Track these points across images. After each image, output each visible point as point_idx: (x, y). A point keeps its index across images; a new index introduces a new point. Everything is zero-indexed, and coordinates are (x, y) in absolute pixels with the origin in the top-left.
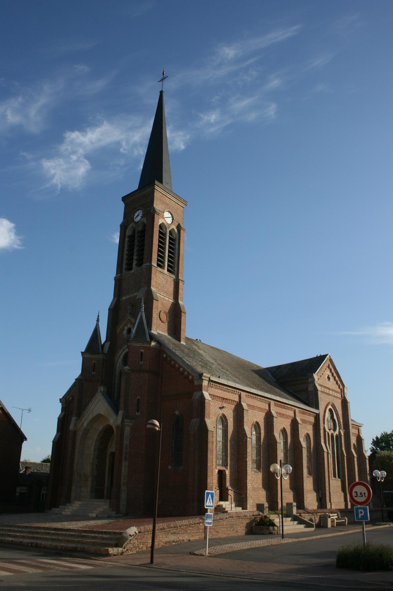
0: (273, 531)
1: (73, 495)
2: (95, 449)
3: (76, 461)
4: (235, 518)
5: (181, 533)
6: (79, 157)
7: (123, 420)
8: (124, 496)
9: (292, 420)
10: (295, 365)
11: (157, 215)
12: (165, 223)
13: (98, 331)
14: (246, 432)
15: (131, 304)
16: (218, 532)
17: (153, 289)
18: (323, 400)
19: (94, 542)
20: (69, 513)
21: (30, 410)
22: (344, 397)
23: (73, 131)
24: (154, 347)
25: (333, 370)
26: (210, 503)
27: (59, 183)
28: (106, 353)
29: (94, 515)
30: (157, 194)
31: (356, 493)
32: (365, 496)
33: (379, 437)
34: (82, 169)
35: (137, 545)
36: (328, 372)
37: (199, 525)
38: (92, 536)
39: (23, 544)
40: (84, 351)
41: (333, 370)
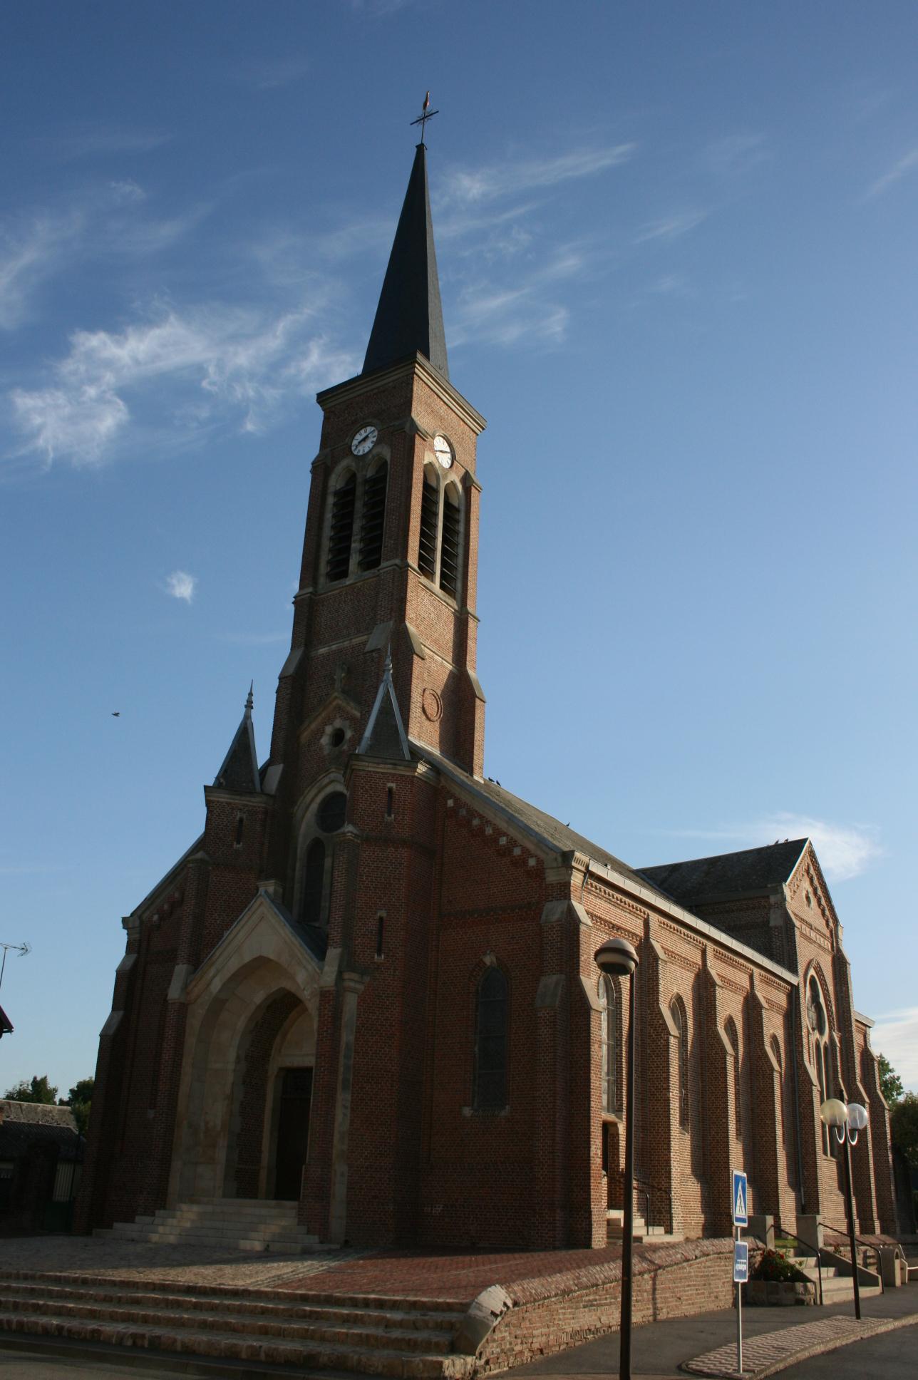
0: (805, 1294)
1: (175, 1185)
2: (238, 1057)
3: (184, 1089)
4: (711, 1257)
6: (104, 392)
7: (340, 973)
8: (339, 1190)
9: (745, 998)
10: (720, 863)
11: (420, 438)
13: (250, 730)
15: (344, 666)
16: (680, 1299)
17: (411, 628)
18: (805, 952)
19: (367, 1336)
20: (172, 1239)
21: (25, 950)
22: (839, 950)
23: (92, 328)
24: (423, 778)
25: (815, 878)
27: (50, 449)
28: (273, 792)
29: (258, 1246)
30: (419, 389)
34: (109, 420)
35: (508, 1346)
36: (806, 885)
37: (641, 1280)
38: (342, 1315)
39: (102, 1338)
40: (211, 785)
41: (815, 878)
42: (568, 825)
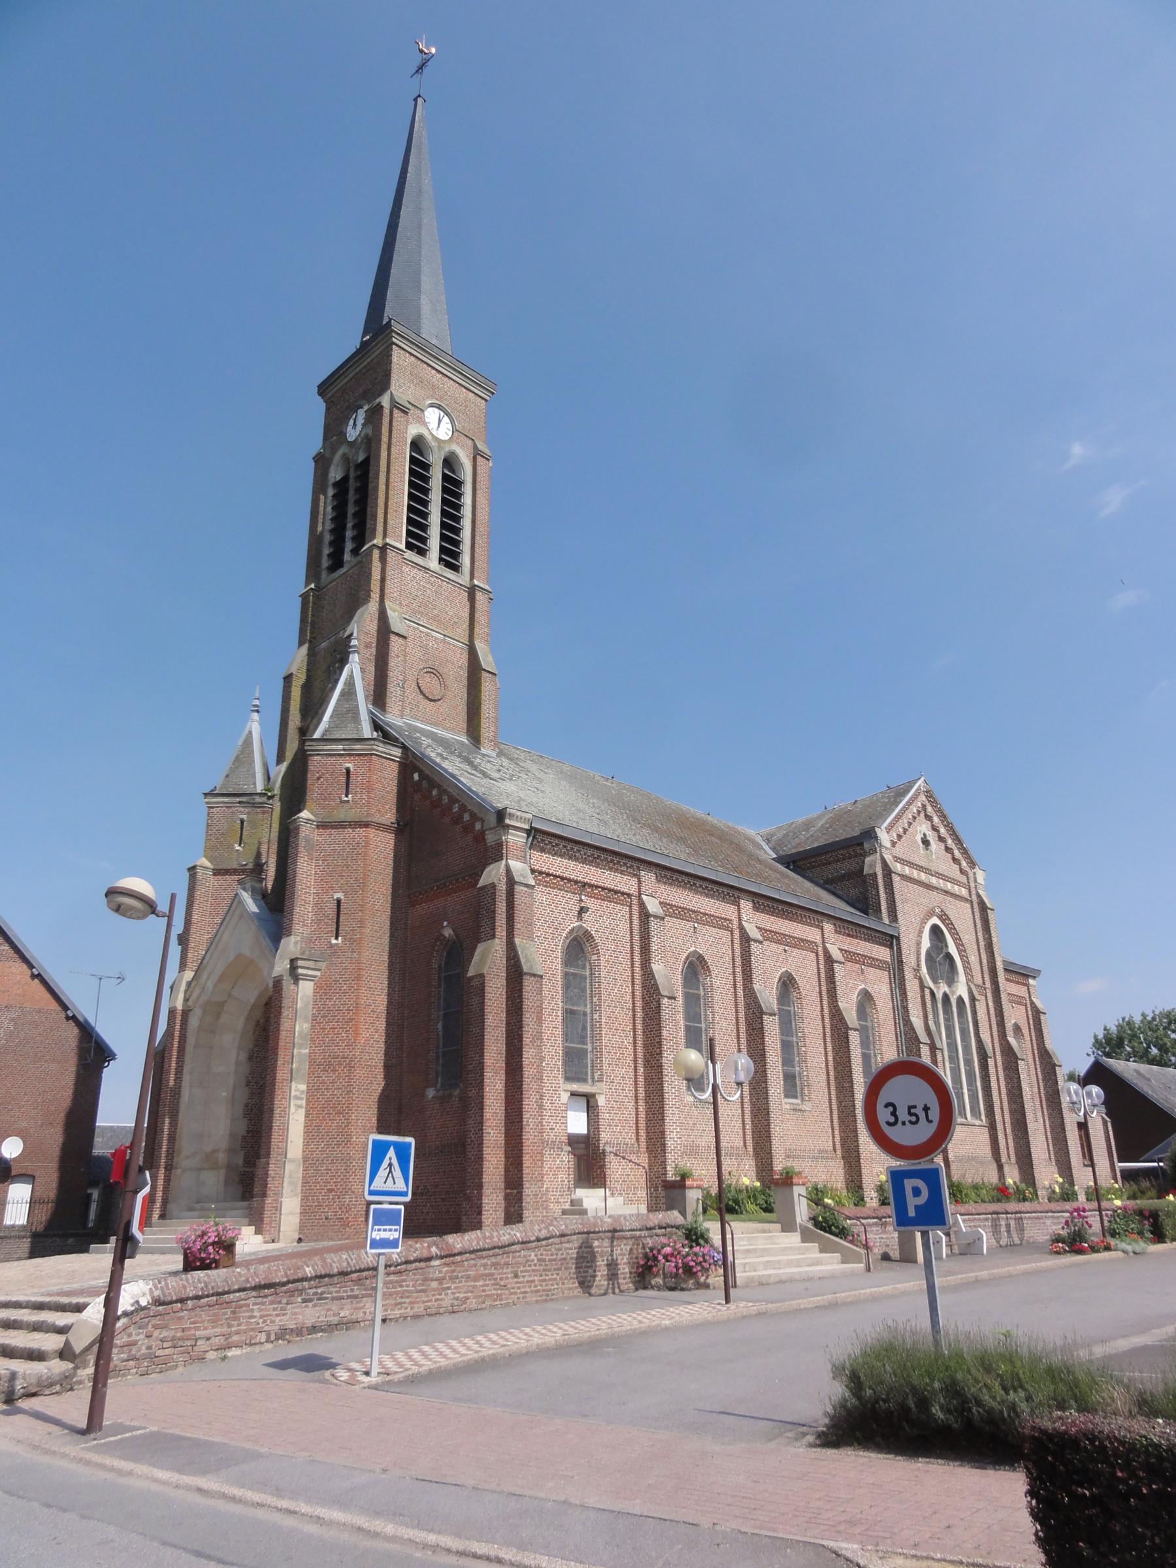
5: (349, 1297)
12: (429, 437)
14: (655, 981)
21: (121, 978)
25: (936, 819)
26: (390, 1179)
31: (891, 1109)
32: (930, 1122)
33: (1114, 1029)
35: (144, 1350)
42: (826, 808)
